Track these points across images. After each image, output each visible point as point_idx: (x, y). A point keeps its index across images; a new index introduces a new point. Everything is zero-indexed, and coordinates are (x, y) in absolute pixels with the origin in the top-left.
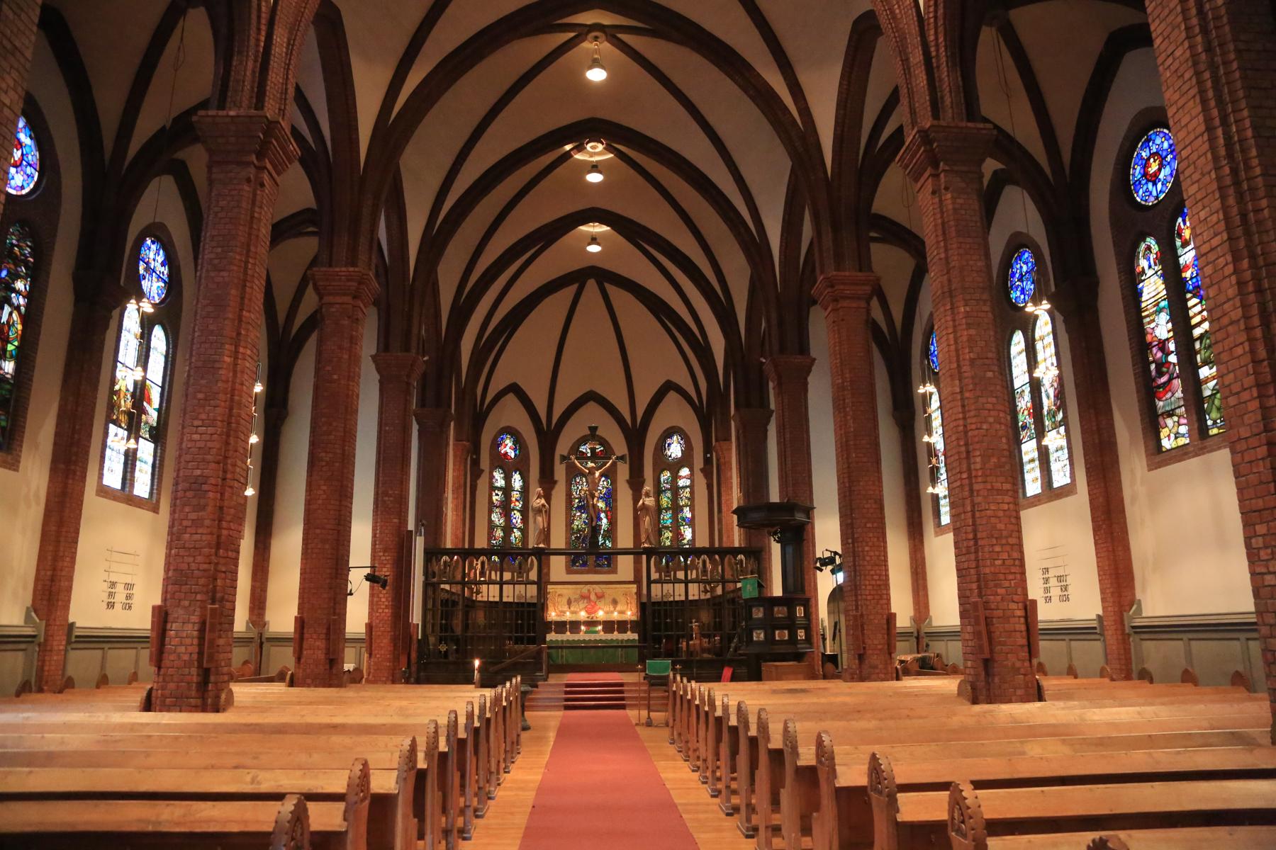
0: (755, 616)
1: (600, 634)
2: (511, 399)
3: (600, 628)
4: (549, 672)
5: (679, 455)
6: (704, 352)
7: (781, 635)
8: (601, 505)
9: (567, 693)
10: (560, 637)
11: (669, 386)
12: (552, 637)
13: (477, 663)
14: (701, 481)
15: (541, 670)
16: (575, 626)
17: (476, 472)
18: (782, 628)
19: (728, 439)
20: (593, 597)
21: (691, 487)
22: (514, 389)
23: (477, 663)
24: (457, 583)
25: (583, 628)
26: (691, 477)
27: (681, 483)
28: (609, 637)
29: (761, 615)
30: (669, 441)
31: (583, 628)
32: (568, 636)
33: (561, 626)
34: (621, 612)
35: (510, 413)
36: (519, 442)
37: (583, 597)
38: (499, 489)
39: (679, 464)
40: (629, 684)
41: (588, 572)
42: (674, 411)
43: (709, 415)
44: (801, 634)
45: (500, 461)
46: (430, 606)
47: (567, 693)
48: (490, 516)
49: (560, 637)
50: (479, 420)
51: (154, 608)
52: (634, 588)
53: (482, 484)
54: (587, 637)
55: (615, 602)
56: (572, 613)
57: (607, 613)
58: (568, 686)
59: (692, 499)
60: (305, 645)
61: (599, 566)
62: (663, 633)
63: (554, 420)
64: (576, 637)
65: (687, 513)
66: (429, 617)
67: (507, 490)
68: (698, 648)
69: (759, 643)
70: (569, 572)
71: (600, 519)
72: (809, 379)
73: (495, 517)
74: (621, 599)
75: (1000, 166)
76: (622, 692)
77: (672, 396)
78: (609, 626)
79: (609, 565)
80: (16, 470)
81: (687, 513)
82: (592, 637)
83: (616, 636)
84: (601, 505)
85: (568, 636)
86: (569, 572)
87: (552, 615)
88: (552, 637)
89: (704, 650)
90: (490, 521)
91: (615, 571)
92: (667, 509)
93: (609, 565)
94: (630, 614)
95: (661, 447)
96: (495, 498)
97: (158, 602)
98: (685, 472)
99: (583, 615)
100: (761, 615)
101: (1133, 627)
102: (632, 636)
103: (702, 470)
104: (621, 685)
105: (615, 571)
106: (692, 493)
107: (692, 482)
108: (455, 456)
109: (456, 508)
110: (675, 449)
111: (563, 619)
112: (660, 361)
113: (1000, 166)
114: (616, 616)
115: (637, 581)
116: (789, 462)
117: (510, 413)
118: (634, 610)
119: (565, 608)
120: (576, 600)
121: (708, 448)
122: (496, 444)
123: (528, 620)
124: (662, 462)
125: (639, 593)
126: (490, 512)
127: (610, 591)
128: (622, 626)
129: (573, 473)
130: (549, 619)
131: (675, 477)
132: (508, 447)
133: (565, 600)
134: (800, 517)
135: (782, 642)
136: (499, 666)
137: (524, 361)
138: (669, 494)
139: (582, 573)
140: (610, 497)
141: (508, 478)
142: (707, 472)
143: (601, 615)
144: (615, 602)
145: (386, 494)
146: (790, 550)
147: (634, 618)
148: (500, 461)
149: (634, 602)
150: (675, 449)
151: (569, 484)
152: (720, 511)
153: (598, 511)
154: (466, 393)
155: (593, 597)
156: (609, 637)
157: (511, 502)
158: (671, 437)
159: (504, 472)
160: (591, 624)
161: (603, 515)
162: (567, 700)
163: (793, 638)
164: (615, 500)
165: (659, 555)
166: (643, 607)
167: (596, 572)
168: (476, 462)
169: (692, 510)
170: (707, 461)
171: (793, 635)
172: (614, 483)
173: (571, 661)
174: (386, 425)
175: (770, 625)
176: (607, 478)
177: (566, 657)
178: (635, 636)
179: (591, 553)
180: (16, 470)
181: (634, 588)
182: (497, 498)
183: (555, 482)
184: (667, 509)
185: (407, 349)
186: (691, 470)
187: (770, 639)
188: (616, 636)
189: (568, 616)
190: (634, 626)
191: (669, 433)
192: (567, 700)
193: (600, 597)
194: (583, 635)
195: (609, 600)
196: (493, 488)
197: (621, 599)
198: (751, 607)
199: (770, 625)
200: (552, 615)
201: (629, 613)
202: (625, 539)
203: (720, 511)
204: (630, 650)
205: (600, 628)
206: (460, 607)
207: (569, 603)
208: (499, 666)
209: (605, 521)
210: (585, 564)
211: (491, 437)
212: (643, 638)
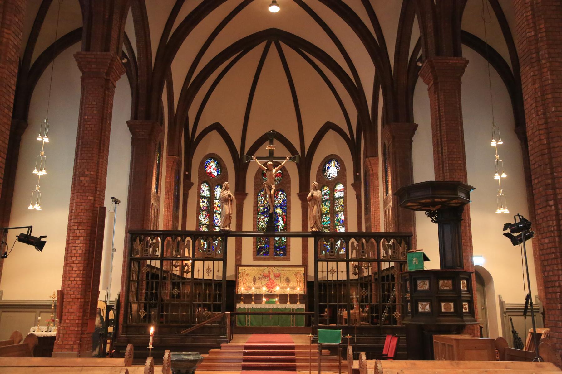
0: (419, 288)
1: (276, 304)
2: (215, 134)
3: (277, 299)
4: (232, 333)
5: (336, 175)
6: (356, 92)
7: (447, 307)
8: (279, 211)
9: (245, 354)
10: (247, 306)
11: (329, 126)
12: (240, 305)
13: (152, 330)
14: (352, 193)
15: (225, 333)
16: (258, 297)
17: (188, 185)
18: (447, 300)
19: (376, 155)
20: (272, 276)
21: (345, 197)
22: (217, 127)
23: (152, 330)
24: (157, 259)
25: (264, 299)
26: (345, 190)
27: (337, 195)
28: (283, 306)
29: (426, 287)
30: (328, 165)
31: (264, 299)
32: (253, 305)
33: (248, 298)
35: (214, 143)
36: (220, 165)
37: (265, 276)
38: (205, 197)
39: (336, 181)
40: (299, 347)
41: (268, 259)
42: (332, 144)
43: (359, 142)
44: (465, 307)
45: (206, 178)
46: (134, 277)
47: (245, 354)
48: (198, 217)
49: (247, 306)
50: (191, 147)
51: (58, 291)
52: (302, 270)
53: (193, 193)
54: (267, 306)
55: (288, 280)
56: (257, 288)
57: (282, 288)
58: (246, 347)
59: (345, 206)
60: (65, 311)
61: (277, 254)
62: (327, 303)
63: (247, 149)
64: (259, 306)
65: (341, 217)
66: (133, 288)
67: (211, 199)
68: (358, 317)
69: (424, 314)
70: (255, 258)
71: (278, 221)
72: (462, 79)
73: (201, 218)
74: (293, 278)
76: (293, 354)
77: (331, 133)
78: (283, 298)
79: (284, 254)
81: (341, 217)
82: (271, 306)
83: (289, 305)
84: (279, 211)
85: (253, 305)
86: (255, 258)
87: (242, 289)
88: (240, 305)
89: (363, 319)
90: (198, 220)
91: (288, 259)
92: (326, 214)
93: (284, 254)
95: (323, 169)
96: (202, 204)
97: (60, 288)
98: (340, 187)
99: (264, 290)
100: (426, 287)
101: (507, 309)
102: (461, 276)
103: (352, 185)
104: (293, 347)
105: (288, 259)
106: (345, 202)
107: (345, 193)
108: (168, 167)
109: (168, 206)
110: (333, 171)
111: (250, 292)
112: (323, 105)
114: (288, 291)
115: (305, 264)
116: (445, 150)
117: (214, 143)
118: (302, 286)
119: (252, 284)
120: (260, 279)
121: (357, 168)
122: (203, 166)
123: (224, 293)
124: (324, 181)
125: (306, 274)
126: (198, 214)
127: (285, 272)
128: (293, 298)
129: (259, 188)
130: (239, 292)
131: (333, 190)
132: (212, 168)
133: (251, 278)
134: (462, 195)
135: (447, 314)
136: (189, 330)
137: (224, 105)
138: (328, 203)
139: (265, 259)
140: (286, 206)
141: (212, 190)
142: (356, 186)
143: (277, 290)
144: (288, 280)
145: (83, 175)
146: (448, 229)
147: (302, 292)
148: (206, 178)
149: (302, 280)
150: (333, 171)
151: (256, 196)
153: (277, 215)
154: (179, 120)
155: (272, 276)
156: (283, 306)
157: (214, 207)
158: (329, 162)
159: (209, 186)
160: (270, 296)
161: (280, 218)
162: (245, 361)
163: (458, 311)
164: (289, 208)
165: (323, 240)
166: (309, 285)
167: (274, 259)
168: (188, 177)
169: (345, 215)
170: (357, 178)
171: (458, 307)
172: (288, 195)
173: (255, 324)
174: (85, 115)
175: (436, 297)
176: (283, 192)
177: (251, 321)
178: (303, 306)
179: (271, 242)
181: (302, 270)
182: (203, 204)
183: (246, 194)
184: (326, 214)
185: (107, 50)
186: (345, 185)
187: (435, 310)
188: (289, 305)
189: (253, 291)
190: (302, 298)
191: (328, 160)
192: (245, 361)
193: (277, 276)
194: (264, 305)
195: (283, 278)
196: (200, 197)
197: (293, 278)
198: (415, 281)
199: (436, 297)
201: (299, 289)
202: (296, 226)
204: (299, 316)
205: (277, 299)
206: (169, 280)
207: (254, 280)
208: (189, 330)
209: (281, 223)
210: (266, 253)
211: (200, 160)
212: (310, 307)
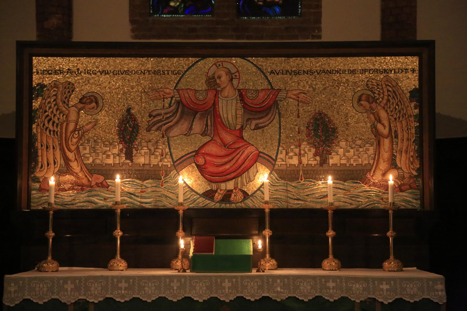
20: (229, 110)
34: (348, 175)
37: (188, 109)
54: (200, 286)
55: (323, 132)
57: (286, 175)
75: (180, 233)
80: (434, 41)
82: (227, 286)
83: (328, 277)
94: (388, 182)
111: (100, 201)
113: (180, 233)
119: (113, 156)
144: (323, 132)
147: (409, 200)
149: (408, 130)
152: (181, 163)
155: (229, 110)
180: (434, 41)
193: (259, 109)
197: (354, 120)
200: (53, 185)
203: (181, 163)
207: (128, 132)
